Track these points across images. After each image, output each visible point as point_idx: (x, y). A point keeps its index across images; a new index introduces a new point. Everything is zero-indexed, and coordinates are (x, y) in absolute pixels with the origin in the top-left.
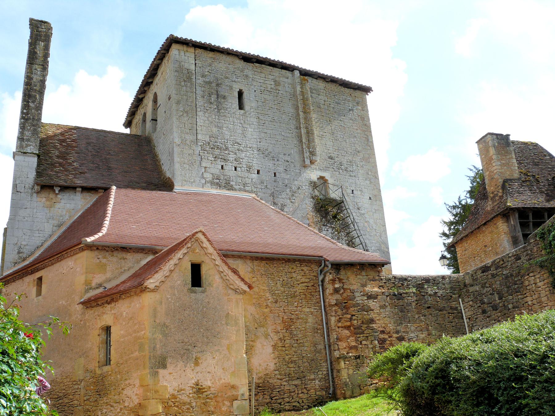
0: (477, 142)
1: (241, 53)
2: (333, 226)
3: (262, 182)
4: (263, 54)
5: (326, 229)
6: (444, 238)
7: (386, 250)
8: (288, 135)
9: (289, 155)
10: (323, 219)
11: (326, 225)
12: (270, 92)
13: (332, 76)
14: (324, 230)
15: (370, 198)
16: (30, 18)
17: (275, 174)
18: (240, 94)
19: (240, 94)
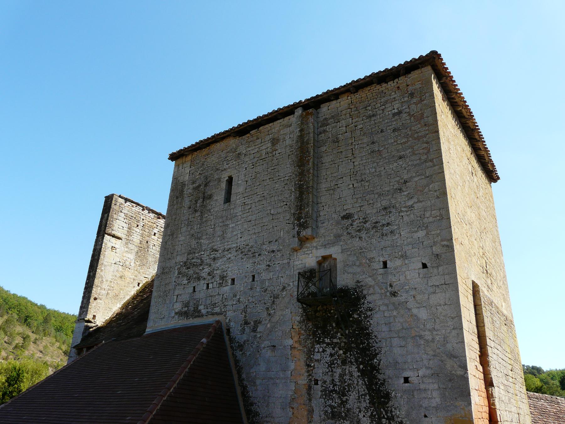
0: (173, 157)
1: (233, 129)
2: (335, 341)
3: (235, 296)
4: (252, 116)
5: (321, 350)
6: (215, 247)
7: (460, 372)
8: (280, 210)
9: (276, 241)
10: (317, 331)
11: (324, 342)
12: (264, 160)
13: (394, 67)
14: (318, 352)
15: (425, 266)
16: (500, 179)
17: (254, 276)
18: (230, 181)
19: (230, 181)
